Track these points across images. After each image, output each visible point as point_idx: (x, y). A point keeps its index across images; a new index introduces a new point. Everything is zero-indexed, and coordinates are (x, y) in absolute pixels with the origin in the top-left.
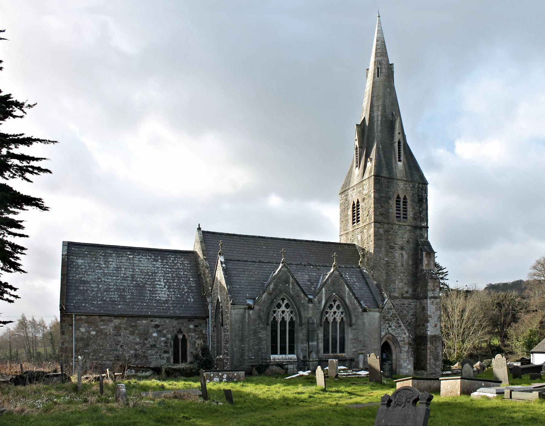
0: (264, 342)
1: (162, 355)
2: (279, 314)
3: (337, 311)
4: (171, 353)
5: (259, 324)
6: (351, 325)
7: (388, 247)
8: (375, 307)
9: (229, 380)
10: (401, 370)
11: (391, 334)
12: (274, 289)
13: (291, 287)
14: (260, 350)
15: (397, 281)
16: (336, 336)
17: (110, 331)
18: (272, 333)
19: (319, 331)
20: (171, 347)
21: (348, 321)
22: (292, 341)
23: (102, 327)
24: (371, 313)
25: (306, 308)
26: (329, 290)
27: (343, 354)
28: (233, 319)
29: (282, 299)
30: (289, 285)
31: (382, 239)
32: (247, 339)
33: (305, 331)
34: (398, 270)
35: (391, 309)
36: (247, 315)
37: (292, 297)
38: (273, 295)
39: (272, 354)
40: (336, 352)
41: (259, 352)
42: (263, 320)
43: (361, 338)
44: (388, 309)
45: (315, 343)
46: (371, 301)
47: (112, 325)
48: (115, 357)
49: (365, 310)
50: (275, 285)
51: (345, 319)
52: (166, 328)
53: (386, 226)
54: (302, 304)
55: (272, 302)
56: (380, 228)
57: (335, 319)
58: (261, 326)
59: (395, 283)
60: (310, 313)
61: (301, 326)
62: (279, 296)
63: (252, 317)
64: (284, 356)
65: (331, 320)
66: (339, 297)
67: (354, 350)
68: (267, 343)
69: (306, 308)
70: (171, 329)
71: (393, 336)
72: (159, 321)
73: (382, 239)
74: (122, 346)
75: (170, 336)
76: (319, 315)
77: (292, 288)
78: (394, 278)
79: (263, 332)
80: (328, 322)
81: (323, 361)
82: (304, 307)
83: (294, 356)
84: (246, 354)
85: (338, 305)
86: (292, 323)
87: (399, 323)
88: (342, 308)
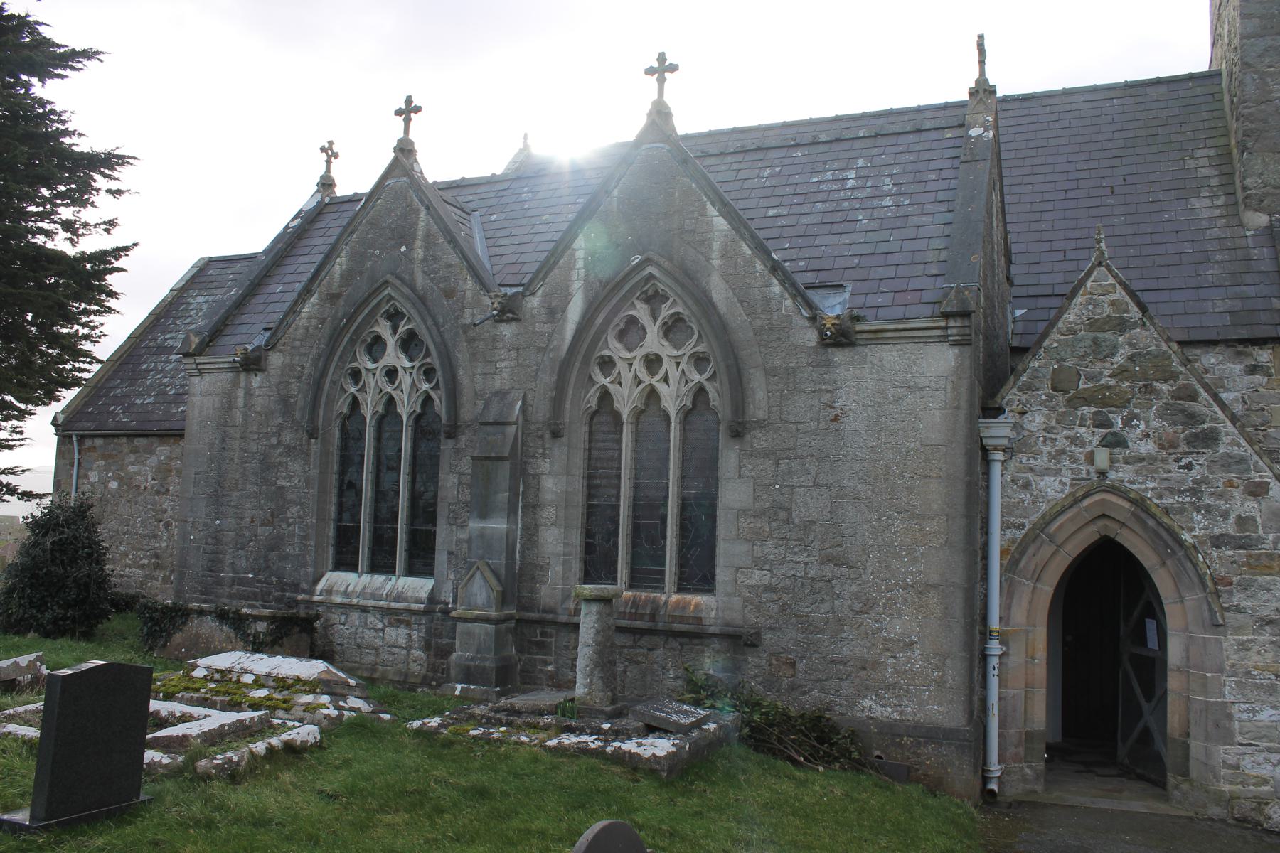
0: (294, 509)
5: (281, 427)
6: (737, 433)
9: (573, 667)
10: (1225, 753)
11: (1114, 490)
12: (347, 277)
14: (276, 544)
17: (146, 480)
19: (544, 465)
22: (424, 512)
23: (131, 469)
24: (889, 356)
25: (481, 346)
29: (647, 300)
30: (410, 249)
32: (235, 495)
35: (1121, 325)
36: (241, 393)
37: (421, 300)
41: (273, 555)
42: (297, 415)
43: (808, 506)
44: (1093, 325)
47: (153, 461)
48: (151, 557)
54: (466, 328)
58: (287, 438)
63: (259, 403)
64: (379, 579)
65: (626, 400)
67: (759, 578)
68: (308, 521)
69: (481, 346)
71: (1139, 503)
74: (168, 525)
77: (425, 260)
79: (295, 466)
82: (470, 341)
83: (420, 587)
84: (228, 559)
85: (677, 319)
86: (424, 424)
87: (1192, 419)
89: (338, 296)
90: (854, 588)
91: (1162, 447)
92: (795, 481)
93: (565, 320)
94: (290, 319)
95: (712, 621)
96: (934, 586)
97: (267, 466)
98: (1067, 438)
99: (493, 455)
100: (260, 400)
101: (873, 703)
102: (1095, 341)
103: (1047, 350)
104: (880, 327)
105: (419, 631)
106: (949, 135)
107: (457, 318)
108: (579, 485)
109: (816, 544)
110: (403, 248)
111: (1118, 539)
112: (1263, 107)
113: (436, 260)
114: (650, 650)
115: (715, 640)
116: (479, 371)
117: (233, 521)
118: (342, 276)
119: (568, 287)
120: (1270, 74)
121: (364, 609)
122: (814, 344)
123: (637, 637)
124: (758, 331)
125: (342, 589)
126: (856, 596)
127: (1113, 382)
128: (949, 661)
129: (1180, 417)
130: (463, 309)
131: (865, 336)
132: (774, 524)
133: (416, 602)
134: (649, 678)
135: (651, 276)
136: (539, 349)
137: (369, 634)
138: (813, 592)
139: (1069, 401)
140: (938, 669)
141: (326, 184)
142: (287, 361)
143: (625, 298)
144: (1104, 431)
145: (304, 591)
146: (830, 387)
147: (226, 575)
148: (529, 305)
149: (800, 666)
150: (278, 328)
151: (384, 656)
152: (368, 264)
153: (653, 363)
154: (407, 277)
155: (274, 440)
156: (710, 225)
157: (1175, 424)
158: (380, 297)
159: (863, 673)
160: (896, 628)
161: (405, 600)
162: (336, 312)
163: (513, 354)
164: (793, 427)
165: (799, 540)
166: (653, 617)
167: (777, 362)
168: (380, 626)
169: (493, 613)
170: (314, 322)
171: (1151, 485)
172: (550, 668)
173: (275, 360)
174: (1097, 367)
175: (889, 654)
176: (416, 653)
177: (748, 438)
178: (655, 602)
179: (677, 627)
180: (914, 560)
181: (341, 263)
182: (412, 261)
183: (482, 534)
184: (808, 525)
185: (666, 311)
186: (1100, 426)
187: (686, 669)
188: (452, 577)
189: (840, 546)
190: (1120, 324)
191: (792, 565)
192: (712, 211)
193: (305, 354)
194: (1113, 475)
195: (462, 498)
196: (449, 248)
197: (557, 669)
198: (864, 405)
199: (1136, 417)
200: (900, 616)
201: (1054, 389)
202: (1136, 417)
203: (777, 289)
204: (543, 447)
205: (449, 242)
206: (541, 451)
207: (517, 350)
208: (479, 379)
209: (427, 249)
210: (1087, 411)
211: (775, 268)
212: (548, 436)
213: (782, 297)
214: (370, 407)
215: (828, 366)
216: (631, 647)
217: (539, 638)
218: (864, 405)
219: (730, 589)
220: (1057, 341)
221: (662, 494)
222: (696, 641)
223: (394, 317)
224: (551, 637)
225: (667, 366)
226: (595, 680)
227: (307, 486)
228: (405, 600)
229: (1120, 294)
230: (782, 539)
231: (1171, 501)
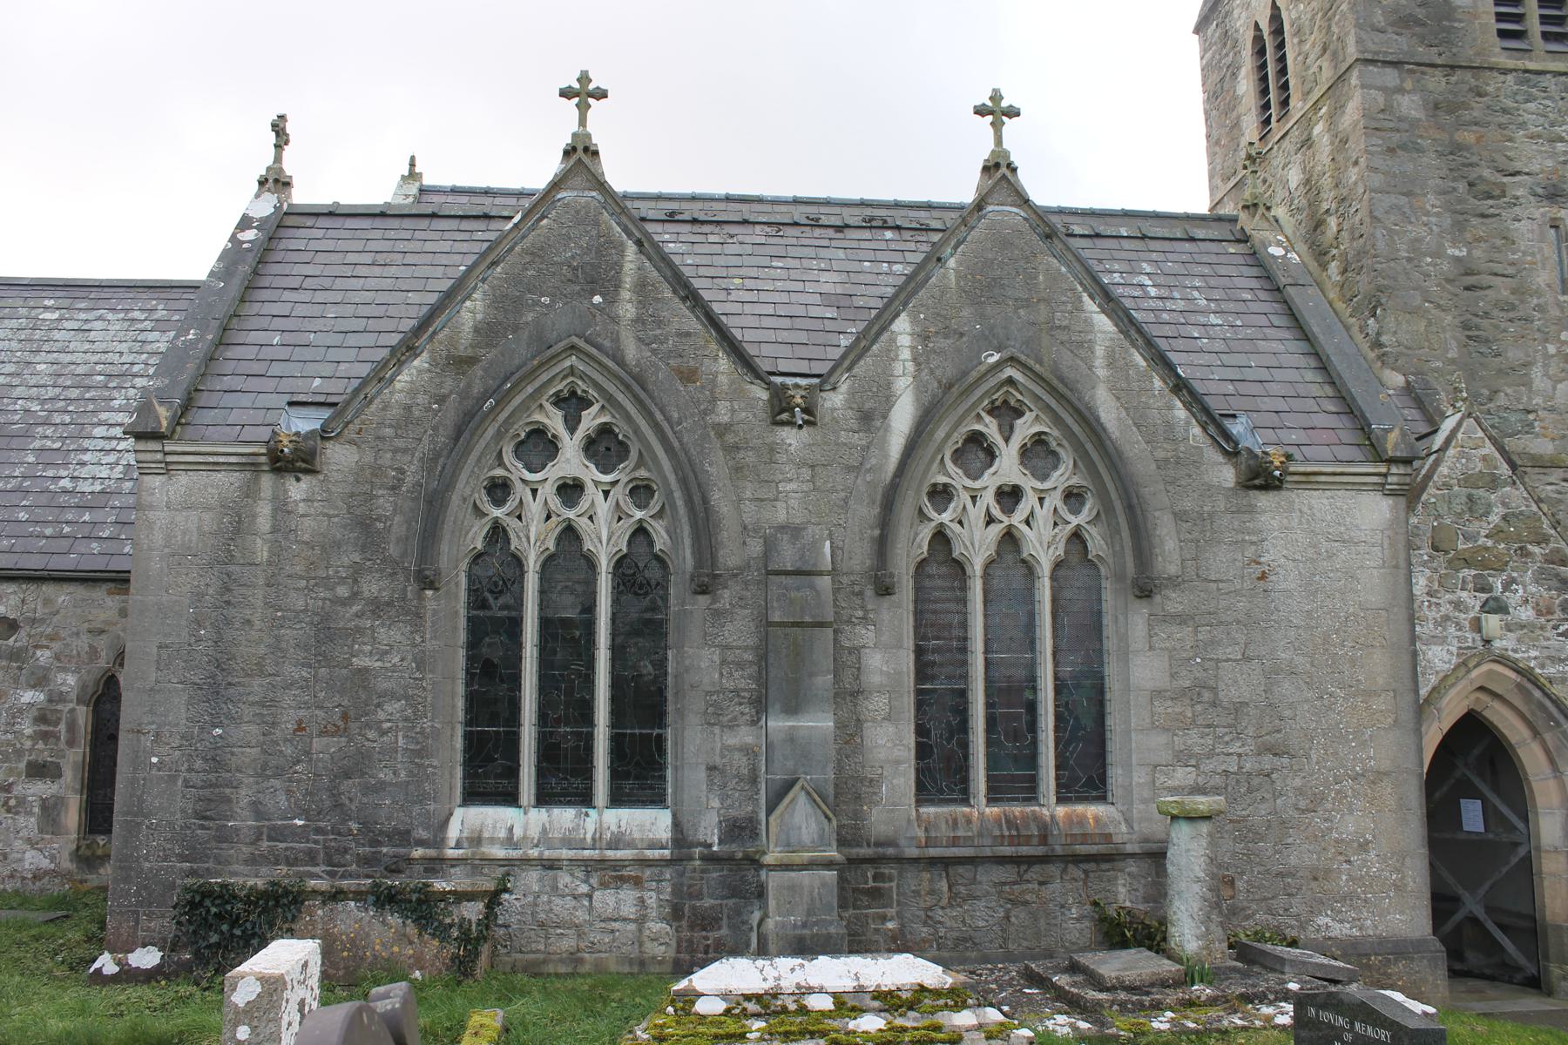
0: (393, 707)
1: (18, 790)
2: (534, 509)
3: (1028, 483)
4: (69, 775)
5: (356, 572)
6: (1145, 590)
7: (1462, 187)
8: (1355, 453)
11: (1502, 660)
12: (488, 332)
13: (627, 309)
14: (354, 766)
15: (1536, 373)
16: (1032, 666)
18: (473, 645)
19: (867, 635)
20: (71, 743)
21: (1125, 552)
22: (644, 704)
24: (1317, 502)
25: (750, 458)
26: (946, 332)
27: (1092, 810)
28: (158, 537)
29: (559, 401)
30: (612, 298)
31: (1420, 150)
32: (257, 685)
33: (740, 631)
34: (1540, 308)
35: (1493, 483)
36: (264, 511)
37: (636, 382)
38: (478, 371)
39: (475, 795)
40: (1030, 791)
42: (393, 550)
43: (1239, 684)
44: (1468, 481)
45: (819, 723)
46: (1320, 420)
49: (1261, 478)
50: (498, 301)
51: (1096, 542)
52: (53, 638)
53: (1436, 82)
54: (722, 430)
55: (467, 424)
56: (1400, 90)
57: (1010, 539)
58: (372, 587)
59: (1528, 384)
60: (790, 501)
61: (703, 590)
63: (308, 528)
64: (565, 816)
65: (977, 544)
66: (1038, 378)
69: (750, 458)
70: (83, 643)
72: (14, 600)
73: (1420, 150)
75: (71, 680)
76: (865, 512)
77: (638, 320)
78: (1514, 355)
79: (392, 634)
80: (959, 568)
81: (900, 860)
83: (653, 823)
84: (244, 796)
85: (1039, 440)
86: (638, 575)
88: (1067, 457)
89: (472, 361)
90: (1298, 782)
91: (1539, 613)
92: (1220, 653)
93: (887, 429)
94: (371, 390)
95: (1126, 838)
96: (1387, 774)
97: (326, 633)
98: (1450, 603)
99: (807, 619)
100: (307, 522)
101: (1327, 920)
102: (1470, 497)
103: (1425, 506)
104: (1316, 469)
105: (658, 892)
106: (1232, 250)
107: (705, 413)
108: (908, 661)
109: (1251, 731)
110: (597, 299)
111: (1487, 714)
112: (1392, 264)
113: (659, 323)
114: (1041, 883)
115: (1131, 861)
116: (748, 494)
117: (254, 729)
118: (476, 330)
119: (889, 385)
120: (1397, 233)
121: (551, 865)
122: (1232, 485)
123: (1024, 867)
124: (1162, 464)
125: (503, 834)
126: (1300, 791)
127: (1490, 543)
128: (1408, 860)
129: (1555, 583)
130: (713, 400)
131: (1296, 478)
132: (1199, 708)
133: (652, 846)
134: (1042, 922)
135: (1010, 381)
136: (849, 469)
137: (563, 906)
138: (1250, 791)
139: (1450, 562)
140: (1398, 871)
141: (275, 181)
142: (369, 458)
143: (610, 399)
144: (1484, 596)
145: (421, 843)
146: (1254, 539)
147: (243, 821)
148: (828, 404)
149: (1240, 884)
150: (348, 403)
151: (595, 937)
152: (530, 317)
153: (570, 490)
154: (607, 343)
155: (343, 591)
156: (1089, 323)
157: (1550, 589)
158: (556, 370)
159: (1314, 884)
160: (1350, 826)
161: (630, 845)
162: (469, 386)
163: (806, 473)
164: (1213, 586)
165: (1229, 726)
166: (1044, 839)
167: (1187, 504)
168: (584, 889)
169: (833, 853)
170: (422, 399)
171: (1533, 653)
172: (890, 925)
173: (339, 457)
174: (1474, 527)
175: (1342, 858)
176: (656, 926)
177: (1158, 598)
178: (1036, 818)
179: (1082, 849)
180: (1363, 745)
181: (473, 310)
182: (615, 320)
183: (791, 738)
184: (1239, 708)
185: (591, 419)
186: (1482, 590)
187: (1095, 904)
188: (716, 803)
189: (1279, 731)
190: (1493, 481)
191: (1222, 758)
192: (1090, 305)
193: (405, 451)
194: (1497, 644)
195: (730, 685)
196: (683, 309)
197: (903, 925)
198: (1294, 560)
199: (1514, 581)
200: (1351, 812)
201: (1435, 548)
202: (1514, 581)
203: (1181, 413)
204: (863, 608)
205: (684, 299)
206: (860, 613)
207: (812, 467)
208: (749, 507)
209: (642, 304)
210: (1468, 573)
211: (1180, 387)
212: (869, 592)
213: (1188, 423)
214: (533, 540)
215: (1251, 512)
216: (1015, 883)
217: (871, 884)
218: (1294, 560)
219: (1146, 794)
220: (1434, 496)
221: (1021, 673)
222: (1104, 866)
223: (572, 404)
224: (891, 880)
225: (592, 494)
226: (1213, 927)
227: (418, 669)
228: (630, 845)
229: (1489, 449)
230: (1209, 726)
231: (1552, 670)
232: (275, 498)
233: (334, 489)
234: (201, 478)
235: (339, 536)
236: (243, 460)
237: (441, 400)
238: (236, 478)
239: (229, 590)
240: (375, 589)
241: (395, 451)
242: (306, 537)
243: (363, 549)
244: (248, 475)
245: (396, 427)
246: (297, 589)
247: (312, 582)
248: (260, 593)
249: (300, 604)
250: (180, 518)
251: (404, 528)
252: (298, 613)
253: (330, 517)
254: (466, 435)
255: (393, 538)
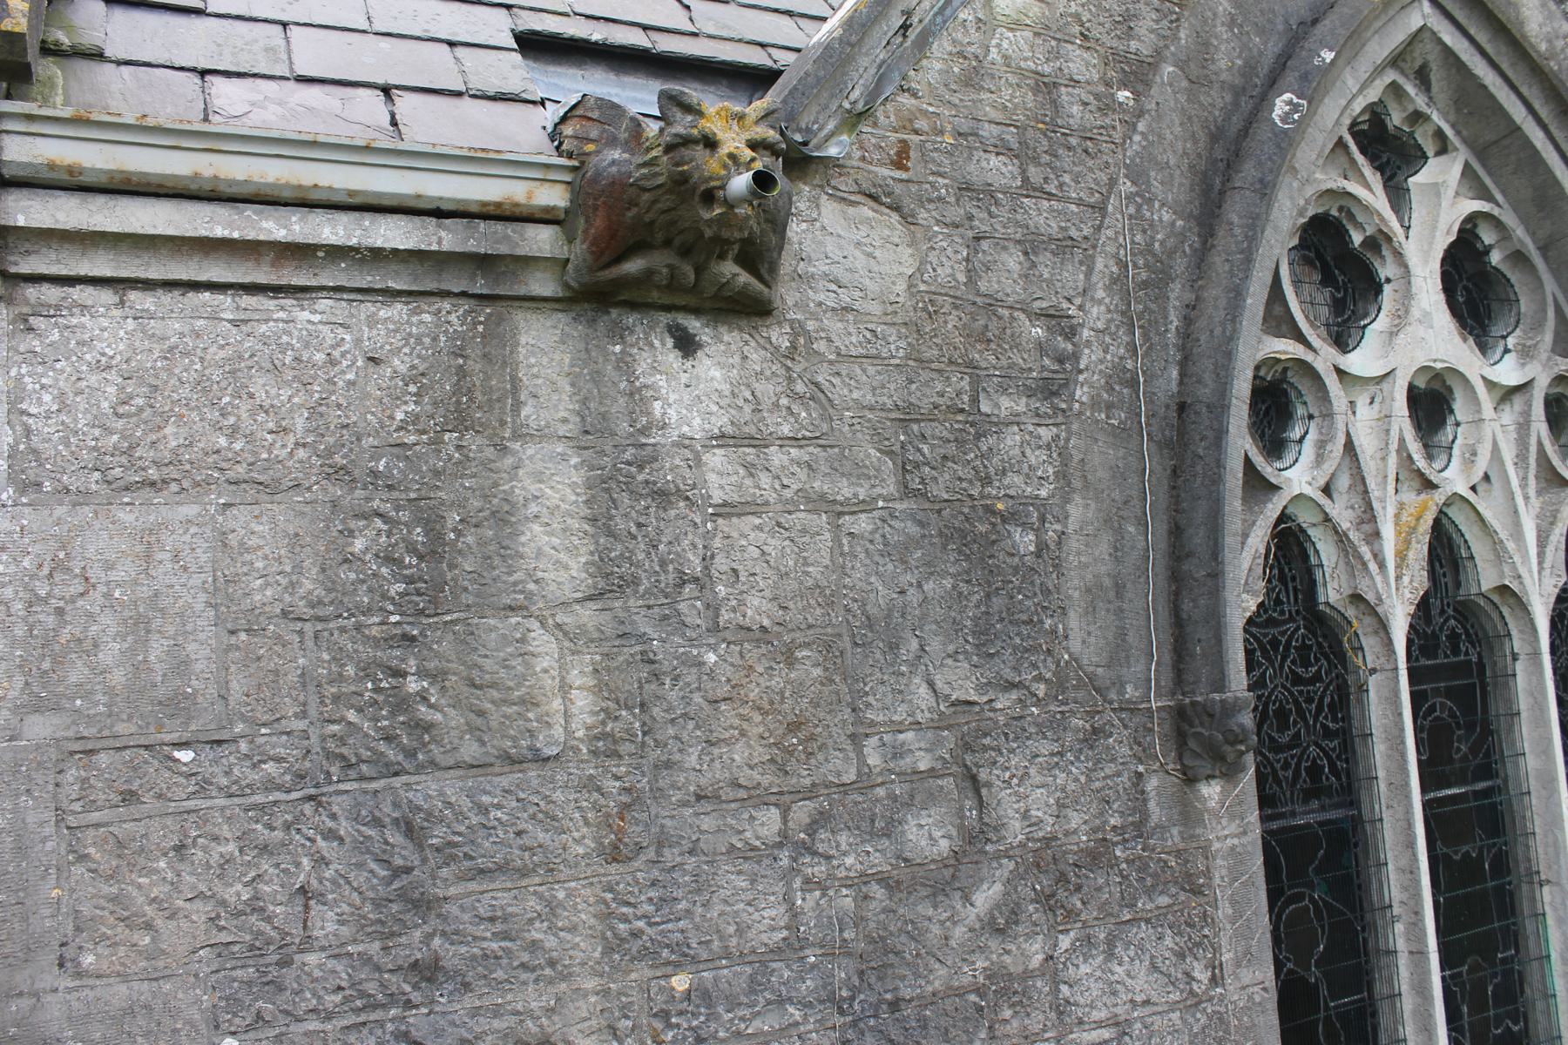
36: (549, 491)
42: (1082, 638)
58: (1035, 796)
62: (1314, 86)
63: (760, 563)
142: (948, 268)
155: (929, 834)
170: (1080, 63)
193: (1064, 246)
221: (1164, 715)
232: (591, 432)
233: (839, 391)
234: (205, 328)
235: (883, 594)
236: (446, 238)
237: (1138, 74)
238: (396, 330)
239: (423, 905)
240: (1040, 802)
241: (1031, 245)
242: (757, 609)
243: (983, 641)
244: (454, 315)
245: (1021, 154)
246: (750, 853)
247: (802, 812)
248: (580, 901)
249: (766, 922)
250: (106, 539)
251: (1103, 548)
252: (761, 961)
253: (836, 510)
254: (1234, 212)
255: (1073, 586)
